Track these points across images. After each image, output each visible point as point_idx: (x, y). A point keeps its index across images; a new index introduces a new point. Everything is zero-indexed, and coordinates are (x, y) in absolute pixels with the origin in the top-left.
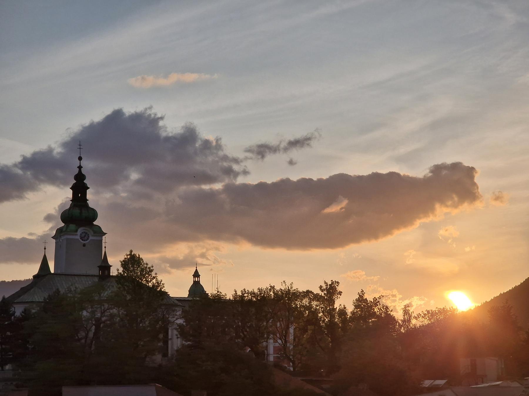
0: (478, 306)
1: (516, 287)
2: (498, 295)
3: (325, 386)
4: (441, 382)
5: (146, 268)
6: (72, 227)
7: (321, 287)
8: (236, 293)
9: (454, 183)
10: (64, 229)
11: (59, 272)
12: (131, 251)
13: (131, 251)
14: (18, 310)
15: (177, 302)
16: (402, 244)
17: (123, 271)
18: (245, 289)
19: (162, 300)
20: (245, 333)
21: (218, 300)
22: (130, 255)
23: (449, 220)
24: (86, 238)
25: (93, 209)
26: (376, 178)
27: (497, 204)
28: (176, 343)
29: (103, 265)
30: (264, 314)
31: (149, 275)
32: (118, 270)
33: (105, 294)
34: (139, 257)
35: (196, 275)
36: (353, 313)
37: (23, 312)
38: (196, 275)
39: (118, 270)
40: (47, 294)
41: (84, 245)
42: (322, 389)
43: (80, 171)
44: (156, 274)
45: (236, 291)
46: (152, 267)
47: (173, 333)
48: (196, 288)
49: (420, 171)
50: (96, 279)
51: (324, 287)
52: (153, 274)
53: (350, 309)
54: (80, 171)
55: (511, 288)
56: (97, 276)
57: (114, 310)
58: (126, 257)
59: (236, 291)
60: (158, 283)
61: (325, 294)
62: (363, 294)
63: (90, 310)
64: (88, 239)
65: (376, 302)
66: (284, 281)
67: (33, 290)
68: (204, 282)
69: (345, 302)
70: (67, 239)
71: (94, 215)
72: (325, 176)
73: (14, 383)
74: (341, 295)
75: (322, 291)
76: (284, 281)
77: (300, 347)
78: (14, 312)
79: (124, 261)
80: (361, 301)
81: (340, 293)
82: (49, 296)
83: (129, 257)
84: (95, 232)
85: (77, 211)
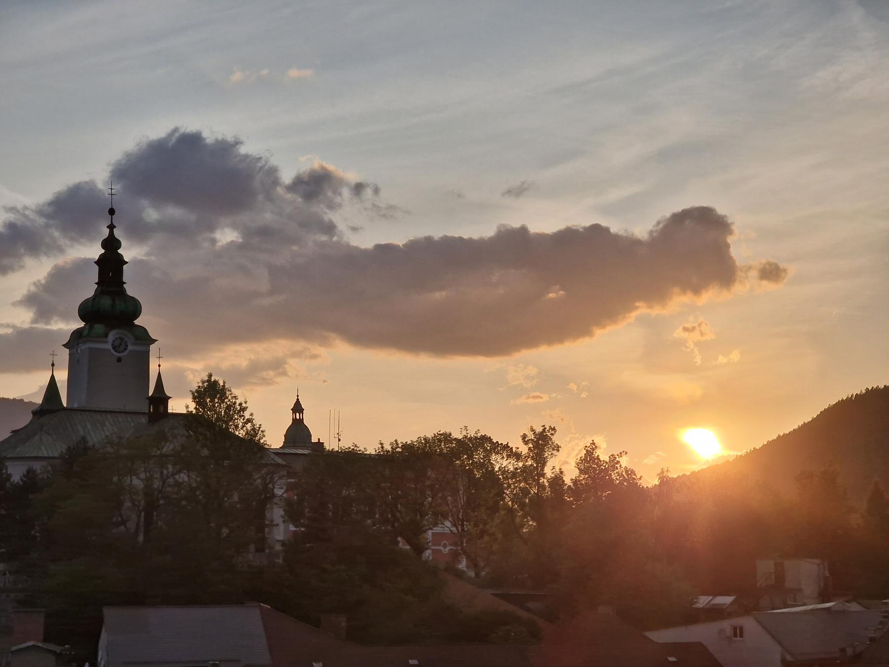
0: (741, 456)
1: (805, 425)
2: (775, 438)
3: (531, 605)
4: (727, 600)
5: (235, 403)
6: (99, 328)
7: (524, 437)
8: (382, 447)
9: (694, 248)
10: (85, 333)
11: (76, 406)
12: (210, 376)
13: (210, 376)
14: (16, 473)
15: (279, 460)
16: (611, 348)
17: (196, 408)
18: (396, 441)
19: (262, 458)
20: (398, 515)
21: (351, 459)
22: (209, 381)
23: (693, 316)
24: (122, 348)
25: (133, 298)
26: (567, 238)
27: (768, 286)
28: (281, 530)
29: (157, 396)
30: (428, 483)
31: (241, 416)
32: (187, 407)
33: (168, 448)
34: (224, 386)
35: (298, 408)
36: (575, 482)
37: (24, 476)
38: (298, 408)
39: (187, 407)
40: (65, 447)
41: (119, 360)
42: (528, 610)
43: (111, 233)
44: (251, 415)
45: (381, 444)
46: (246, 403)
47: (277, 513)
48: (298, 431)
49: (641, 227)
50: (144, 420)
51: (531, 436)
52: (247, 415)
53: (571, 474)
54: (111, 233)
55: (796, 427)
56: (144, 413)
57: (182, 475)
58: (201, 385)
59: (381, 444)
60: (254, 429)
61: (530, 449)
62: (593, 449)
63: (143, 476)
64: (123, 352)
65: (614, 461)
66: (466, 427)
67: (37, 437)
68: (309, 420)
69: (564, 464)
70: (91, 349)
71: (135, 309)
72: (476, 236)
73: (12, 596)
74: (558, 451)
75: (526, 443)
76: (466, 427)
77: (486, 538)
78: (10, 476)
79: (197, 391)
80: (589, 460)
81: (558, 448)
82: (69, 448)
83: (205, 384)
84: (137, 338)
85: (106, 302)
